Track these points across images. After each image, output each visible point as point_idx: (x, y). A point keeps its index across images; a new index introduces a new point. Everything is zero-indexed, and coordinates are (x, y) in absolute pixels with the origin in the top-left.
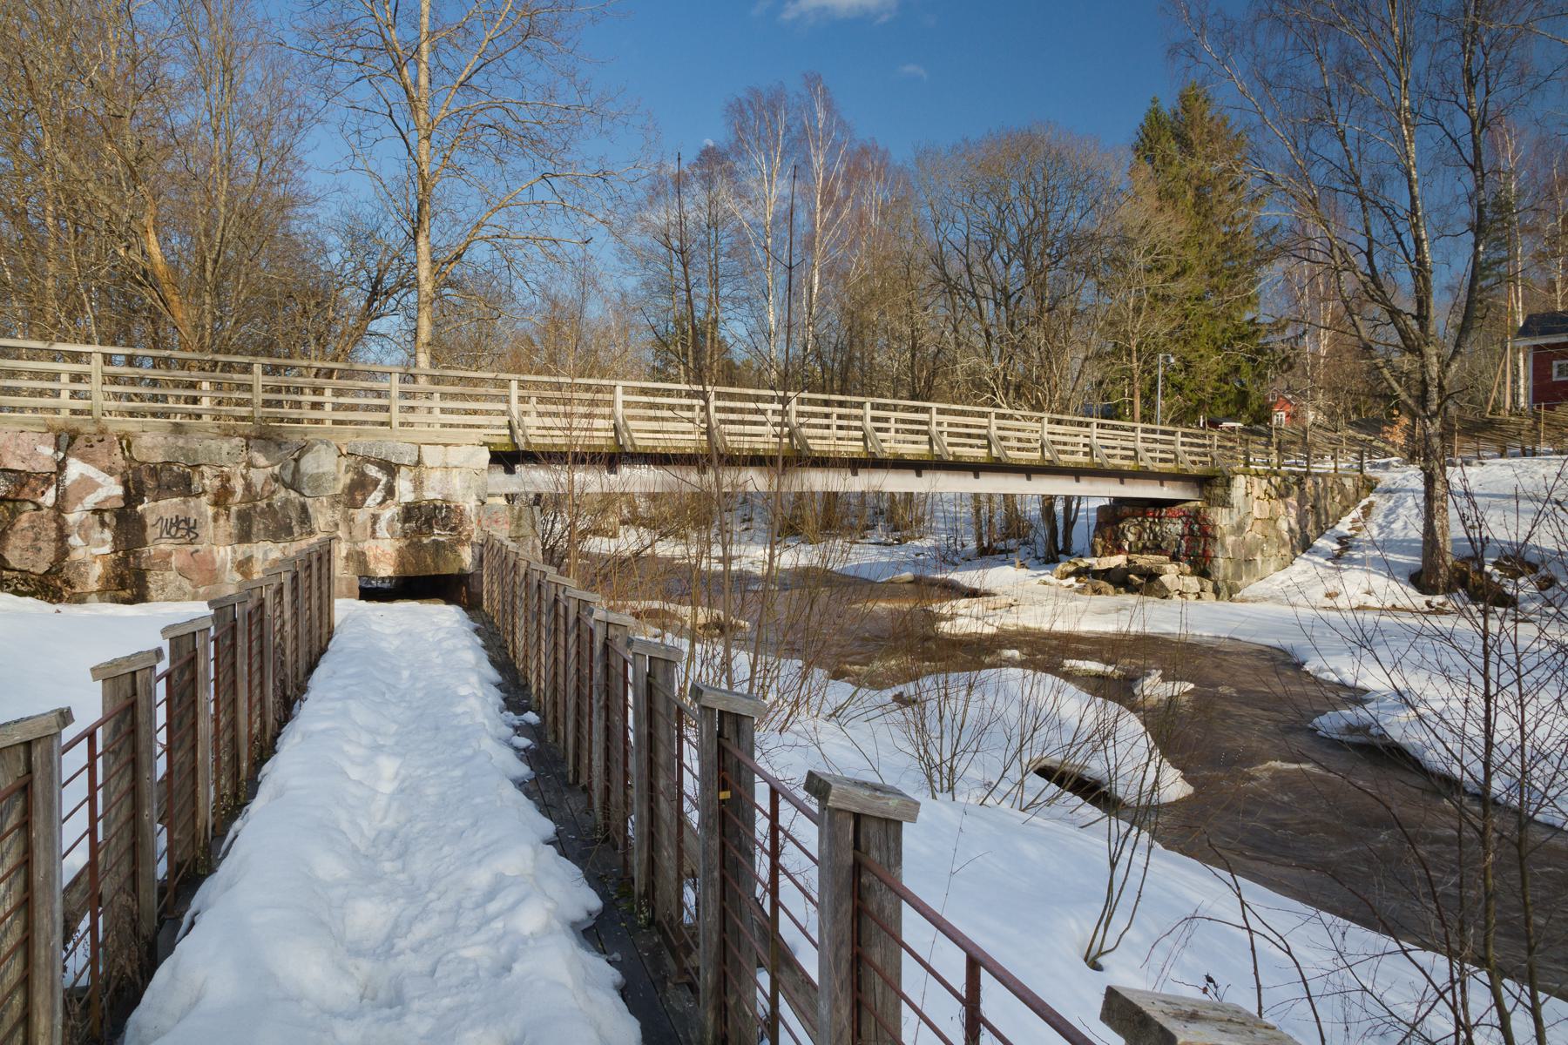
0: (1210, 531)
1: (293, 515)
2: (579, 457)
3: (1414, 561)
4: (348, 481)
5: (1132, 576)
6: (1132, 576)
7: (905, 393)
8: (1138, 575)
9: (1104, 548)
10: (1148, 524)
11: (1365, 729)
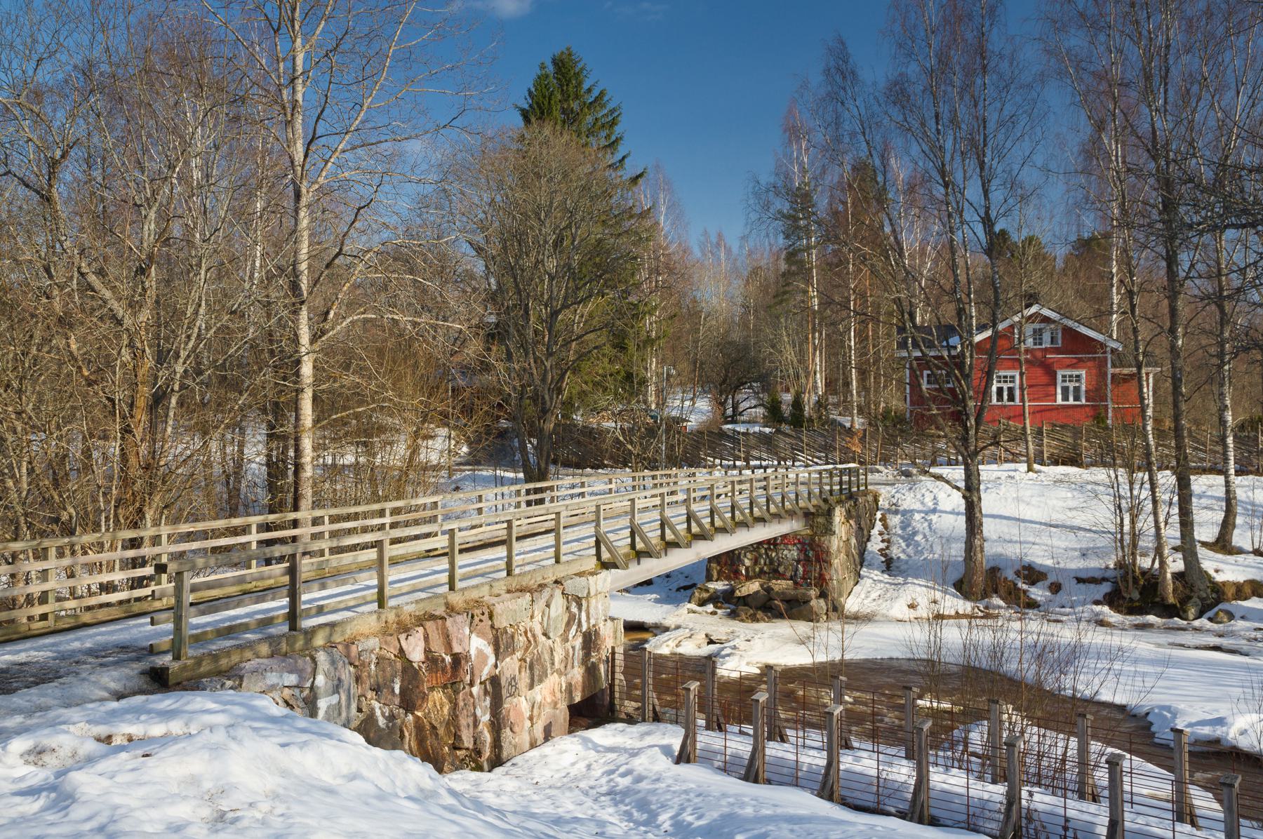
2: (67, 552)
7: (1051, 388)
9: (719, 573)
11: (1217, 741)
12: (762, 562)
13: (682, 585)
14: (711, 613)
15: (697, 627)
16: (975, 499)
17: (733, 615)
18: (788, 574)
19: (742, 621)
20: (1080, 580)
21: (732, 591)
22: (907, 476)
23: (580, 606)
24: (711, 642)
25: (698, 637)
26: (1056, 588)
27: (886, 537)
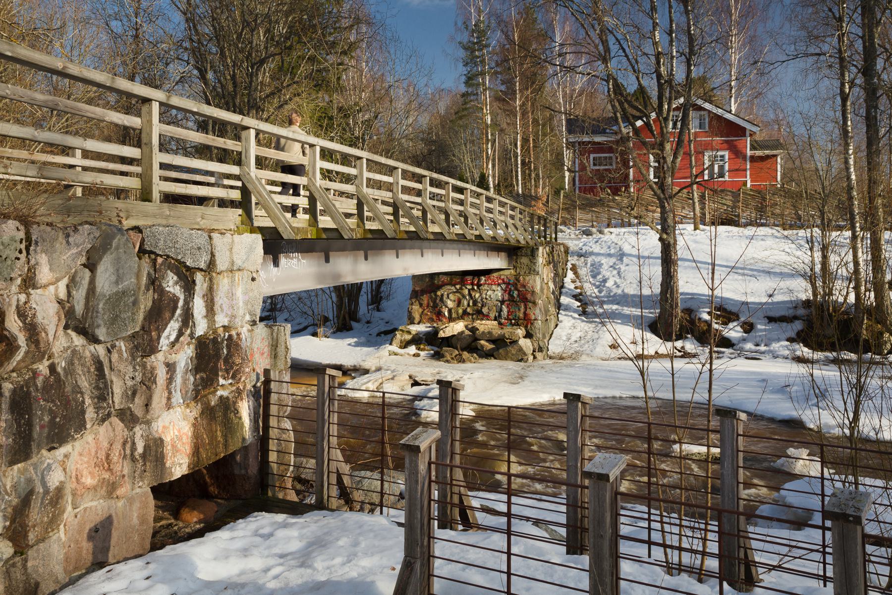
0: (529, 296)
1: (84, 383)
3: (652, 313)
4: (150, 304)
5: (482, 342)
6: (482, 342)
8: (488, 341)
10: (466, 292)
12: (466, 303)
13: (383, 329)
14: (414, 355)
15: (400, 368)
16: (672, 242)
17: (437, 356)
18: (492, 315)
19: (447, 361)
20: (771, 320)
21: (436, 332)
22: (587, 235)
23: (189, 287)
24: (416, 383)
25: (401, 378)
26: (749, 328)
27: (578, 284)
